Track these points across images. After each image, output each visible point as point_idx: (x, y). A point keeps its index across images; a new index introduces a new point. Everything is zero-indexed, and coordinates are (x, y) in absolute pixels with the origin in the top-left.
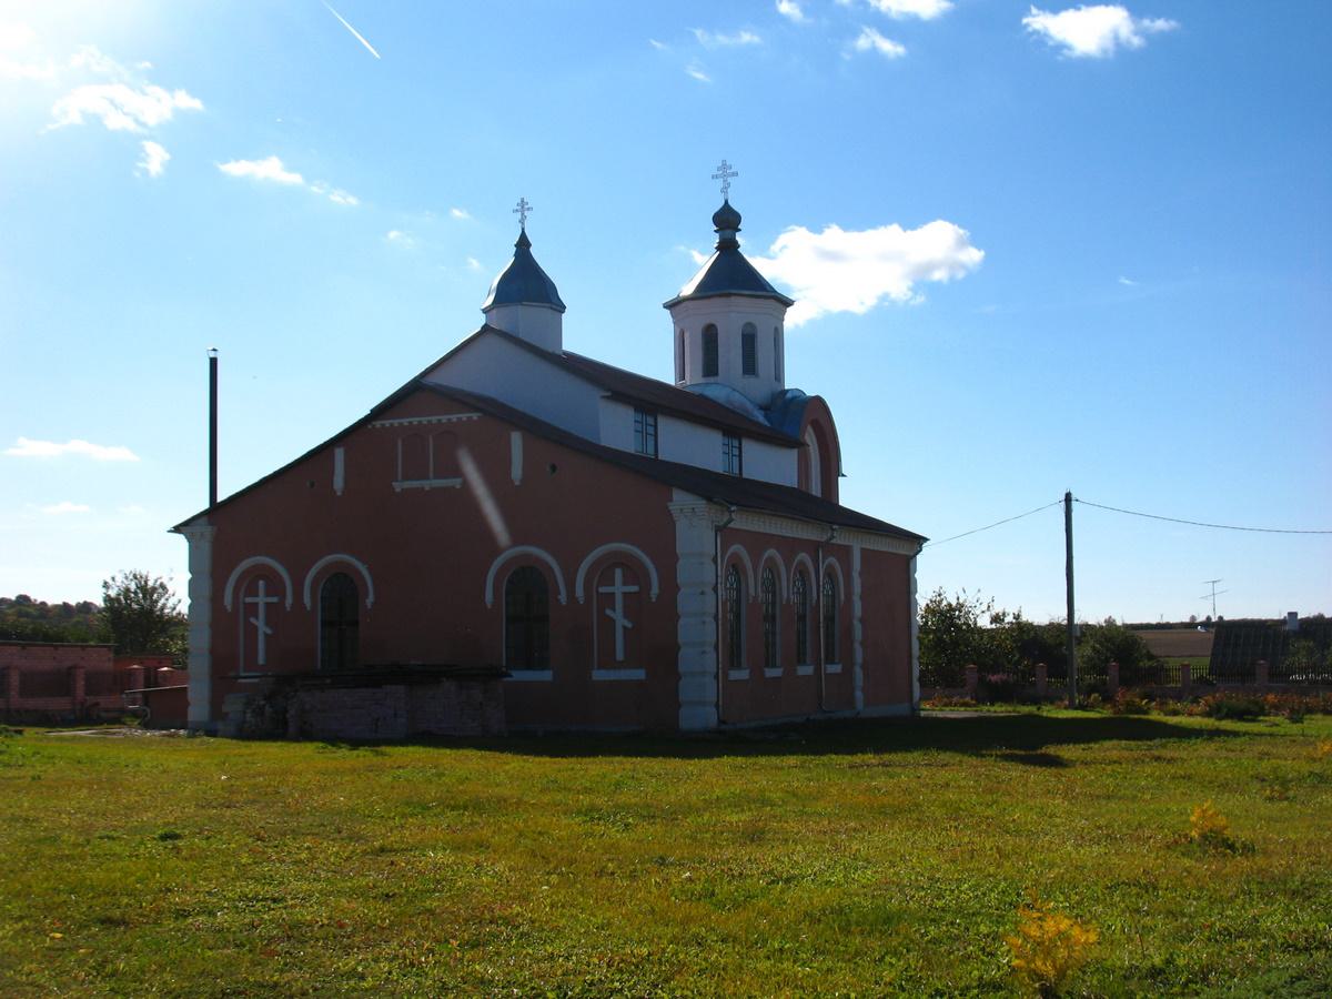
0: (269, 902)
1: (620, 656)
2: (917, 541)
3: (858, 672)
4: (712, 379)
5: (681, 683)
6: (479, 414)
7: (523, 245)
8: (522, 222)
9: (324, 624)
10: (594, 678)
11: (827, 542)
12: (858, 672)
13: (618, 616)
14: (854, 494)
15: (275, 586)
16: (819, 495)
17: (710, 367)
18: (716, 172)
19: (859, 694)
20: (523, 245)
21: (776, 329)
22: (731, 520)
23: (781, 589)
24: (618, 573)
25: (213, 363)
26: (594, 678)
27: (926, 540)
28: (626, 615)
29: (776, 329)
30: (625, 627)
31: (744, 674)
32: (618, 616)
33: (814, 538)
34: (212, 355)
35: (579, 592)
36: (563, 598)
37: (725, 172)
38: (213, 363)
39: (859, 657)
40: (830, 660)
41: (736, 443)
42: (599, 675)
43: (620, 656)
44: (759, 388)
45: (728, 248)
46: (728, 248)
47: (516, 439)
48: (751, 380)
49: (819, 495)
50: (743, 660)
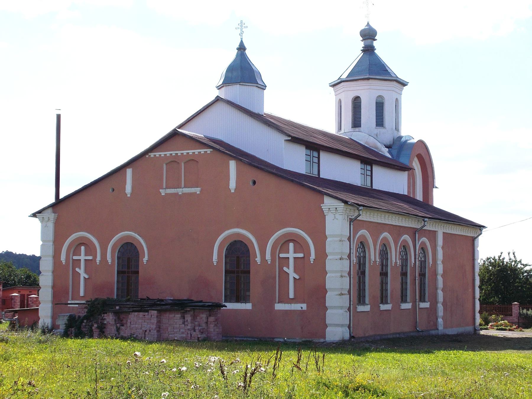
1: (291, 295)
4: (357, 129)
6: (211, 150)
7: (242, 48)
8: (241, 34)
9: (118, 272)
13: (81, 271)
14: (441, 200)
15: (90, 249)
17: (356, 123)
20: (242, 48)
21: (397, 99)
22: (424, 226)
23: (370, 255)
24: (291, 245)
25: (59, 117)
27: (484, 227)
28: (295, 271)
29: (397, 99)
32: (81, 271)
35: (268, 257)
36: (258, 259)
38: (59, 117)
40: (422, 299)
42: (279, 307)
43: (291, 295)
44: (387, 134)
45: (369, 50)
46: (369, 50)
48: (380, 130)
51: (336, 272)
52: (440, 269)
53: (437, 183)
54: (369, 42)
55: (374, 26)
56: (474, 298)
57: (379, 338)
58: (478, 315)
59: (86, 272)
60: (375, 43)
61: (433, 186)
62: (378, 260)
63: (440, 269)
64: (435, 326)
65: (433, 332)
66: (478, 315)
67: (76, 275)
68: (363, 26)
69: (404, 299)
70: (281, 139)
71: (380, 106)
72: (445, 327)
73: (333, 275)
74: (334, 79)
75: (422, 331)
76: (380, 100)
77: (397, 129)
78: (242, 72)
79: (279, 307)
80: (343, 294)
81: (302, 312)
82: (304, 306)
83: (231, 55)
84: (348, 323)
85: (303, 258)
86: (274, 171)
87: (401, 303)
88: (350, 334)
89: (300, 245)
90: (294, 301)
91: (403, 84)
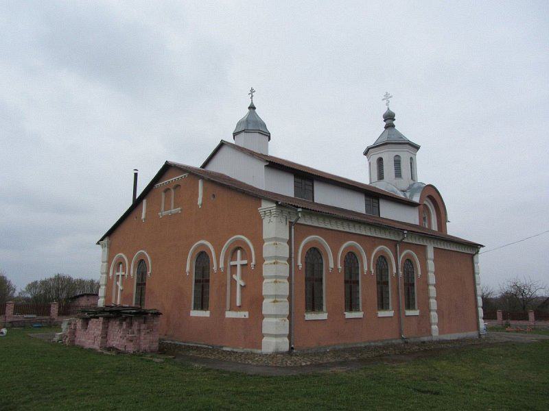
0: (347, 355)
2: (476, 247)
3: (434, 316)
5: (264, 320)
7: (252, 108)
10: (191, 315)
11: (401, 241)
12: (434, 316)
13: (237, 277)
14: (452, 230)
16: (437, 230)
17: (381, 177)
18: (383, 98)
19: (434, 327)
20: (252, 108)
21: (411, 158)
22: (298, 219)
23: (363, 266)
25: (136, 175)
26: (191, 315)
27: (482, 246)
30: (241, 286)
31: (389, 313)
32: (237, 277)
33: (393, 238)
34: (136, 172)
35: (222, 265)
36: (215, 268)
37: (387, 97)
38: (136, 175)
39: (433, 303)
40: (410, 306)
41: (377, 201)
42: (230, 314)
44: (404, 182)
47: (200, 183)
48: (399, 180)
49: (437, 230)
50: (324, 308)
51: (271, 277)
52: (432, 279)
53: (449, 218)
54: (389, 121)
55: (392, 110)
56: (477, 306)
57: (342, 347)
58: (481, 322)
59: (243, 278)
60: (394, 122)
61: (446, 221)
62: (340, 267)
63: (432, 279)
64: (429, 332)
65: (425, 339)
66: (481, 322)
67: (234, 282)
68: (384, 111)
69: (383, 305)
70: (261, 166)
71: (397, 163)
72: (441, 332)
73: (269, 280)
74: (364, 149)
75: (255, 375)
76: (397, 158)
77: (413, 177)
78: (253, 126)
79: (230, 314)
80: (277, 302)
81: (245, 320)
82: (247, 314)
83: (244, 112)
84: (288, 333)
85: (247, 265)
86: (341, 215)
87: (379, 310)
88: (290, 345)
89: (246, 255)
90: (240, 308)
91: (417, 148)
